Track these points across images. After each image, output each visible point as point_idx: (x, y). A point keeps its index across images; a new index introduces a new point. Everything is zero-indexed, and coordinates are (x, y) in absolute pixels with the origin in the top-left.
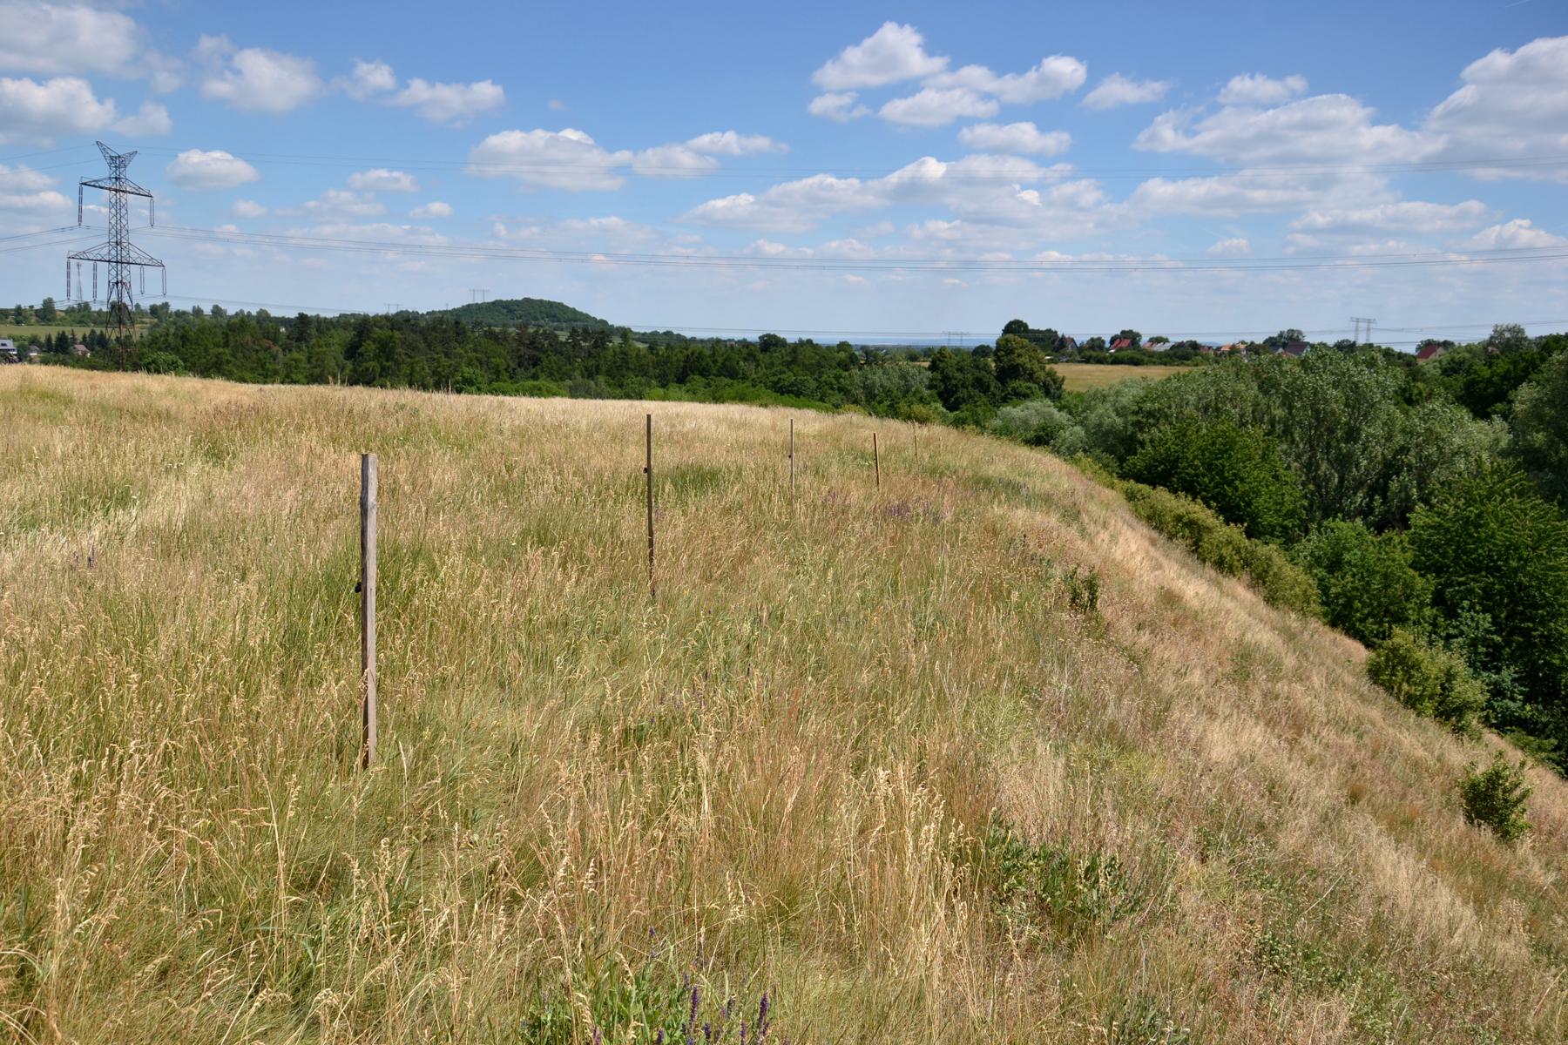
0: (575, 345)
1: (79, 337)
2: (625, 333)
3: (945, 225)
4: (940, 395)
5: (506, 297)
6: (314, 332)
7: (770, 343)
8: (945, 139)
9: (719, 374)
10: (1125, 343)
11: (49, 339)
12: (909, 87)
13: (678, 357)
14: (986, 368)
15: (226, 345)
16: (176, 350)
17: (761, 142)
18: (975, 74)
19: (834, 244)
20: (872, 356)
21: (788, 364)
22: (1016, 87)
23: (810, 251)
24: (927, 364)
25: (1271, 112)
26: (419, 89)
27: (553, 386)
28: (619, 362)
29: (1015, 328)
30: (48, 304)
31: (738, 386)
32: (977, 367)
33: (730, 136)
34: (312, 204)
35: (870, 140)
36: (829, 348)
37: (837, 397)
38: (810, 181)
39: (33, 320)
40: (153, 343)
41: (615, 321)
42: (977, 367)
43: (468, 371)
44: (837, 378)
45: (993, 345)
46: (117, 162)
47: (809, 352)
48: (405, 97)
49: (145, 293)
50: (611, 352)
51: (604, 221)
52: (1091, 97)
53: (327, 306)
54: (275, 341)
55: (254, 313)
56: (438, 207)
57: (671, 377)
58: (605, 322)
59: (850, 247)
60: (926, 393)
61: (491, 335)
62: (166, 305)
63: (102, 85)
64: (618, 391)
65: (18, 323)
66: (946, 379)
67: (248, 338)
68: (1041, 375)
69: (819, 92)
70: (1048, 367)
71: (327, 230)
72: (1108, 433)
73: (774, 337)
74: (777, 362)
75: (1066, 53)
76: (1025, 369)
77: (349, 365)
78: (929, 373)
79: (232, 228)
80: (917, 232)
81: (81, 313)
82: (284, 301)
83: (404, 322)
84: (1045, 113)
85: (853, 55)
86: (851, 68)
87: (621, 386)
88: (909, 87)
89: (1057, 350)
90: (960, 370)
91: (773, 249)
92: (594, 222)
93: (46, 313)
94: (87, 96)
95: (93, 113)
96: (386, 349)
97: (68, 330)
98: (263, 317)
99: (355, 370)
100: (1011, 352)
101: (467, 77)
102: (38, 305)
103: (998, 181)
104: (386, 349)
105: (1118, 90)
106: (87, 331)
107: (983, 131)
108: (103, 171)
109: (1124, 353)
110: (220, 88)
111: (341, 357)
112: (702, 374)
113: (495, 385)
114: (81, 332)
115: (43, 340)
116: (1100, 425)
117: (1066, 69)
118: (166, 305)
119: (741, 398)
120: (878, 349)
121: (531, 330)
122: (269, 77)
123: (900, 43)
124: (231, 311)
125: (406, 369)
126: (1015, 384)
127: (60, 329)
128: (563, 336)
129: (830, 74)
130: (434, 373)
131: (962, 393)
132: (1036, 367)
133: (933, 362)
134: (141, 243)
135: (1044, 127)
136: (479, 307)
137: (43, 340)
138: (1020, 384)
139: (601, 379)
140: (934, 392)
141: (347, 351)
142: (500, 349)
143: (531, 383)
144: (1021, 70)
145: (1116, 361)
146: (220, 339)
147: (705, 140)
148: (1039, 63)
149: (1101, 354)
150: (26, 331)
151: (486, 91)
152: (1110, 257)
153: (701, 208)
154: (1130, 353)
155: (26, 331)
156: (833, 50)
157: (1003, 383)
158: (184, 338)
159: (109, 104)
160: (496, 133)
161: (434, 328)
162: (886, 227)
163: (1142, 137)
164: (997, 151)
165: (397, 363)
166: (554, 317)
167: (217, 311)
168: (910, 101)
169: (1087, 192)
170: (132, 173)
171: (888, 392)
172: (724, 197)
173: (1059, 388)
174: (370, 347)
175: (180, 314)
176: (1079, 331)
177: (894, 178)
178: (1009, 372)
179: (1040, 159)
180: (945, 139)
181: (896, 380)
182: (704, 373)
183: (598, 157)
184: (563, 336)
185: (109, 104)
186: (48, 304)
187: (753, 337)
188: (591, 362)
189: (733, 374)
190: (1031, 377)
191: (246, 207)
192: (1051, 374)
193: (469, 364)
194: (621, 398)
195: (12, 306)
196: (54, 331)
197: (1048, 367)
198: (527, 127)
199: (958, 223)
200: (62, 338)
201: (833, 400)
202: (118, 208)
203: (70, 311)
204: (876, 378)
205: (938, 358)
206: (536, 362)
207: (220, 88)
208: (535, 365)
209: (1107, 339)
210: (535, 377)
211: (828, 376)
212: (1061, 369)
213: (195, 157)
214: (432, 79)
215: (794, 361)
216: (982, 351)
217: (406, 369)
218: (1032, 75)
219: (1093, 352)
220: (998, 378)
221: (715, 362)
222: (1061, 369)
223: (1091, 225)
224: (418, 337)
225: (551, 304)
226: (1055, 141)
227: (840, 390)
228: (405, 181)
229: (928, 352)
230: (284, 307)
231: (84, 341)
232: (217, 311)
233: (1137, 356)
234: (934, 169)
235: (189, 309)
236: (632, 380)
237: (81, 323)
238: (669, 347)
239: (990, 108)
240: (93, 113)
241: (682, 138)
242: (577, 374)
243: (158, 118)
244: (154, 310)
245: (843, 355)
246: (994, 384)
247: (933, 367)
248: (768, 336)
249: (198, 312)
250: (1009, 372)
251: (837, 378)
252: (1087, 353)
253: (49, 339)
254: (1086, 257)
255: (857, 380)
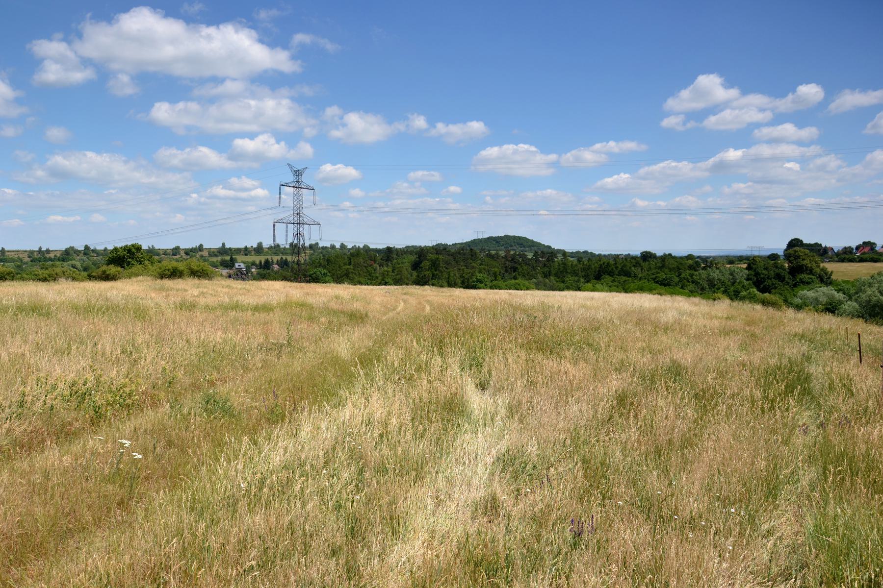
0: (537, 261)
1: (275, 261)
2: (564, 253)
3: (742, 185)
4: (754, 283)
5: (495, 234)
6: (395, 256)
7: (647, 256)
8: (743, 137)
9: (619, 275)
10: (866, 250)
11: (261, 263)
12: (716, 109)
13: (595, 266)
14: (782, 267)
15: (350, 264)
16: (324, 267)
17: (630, 145)
18: (757, 99)
19: (677, 199)
20: (708, 262)
21: (661, 268)
22: (785, 104)
23: (662, 203)
24: (745, 266)
25: (737, 111)
26: (441, 127)
27: (526, 283)
28: (562, 269)
29: (795, 243)
30: (260, 245)
31: (638, 283)
32: (777, 267)
33: (612, 144)
34: (388, 191)
35: (699, 140)
36: (681, 258)
37: (691, 287)
38: (662, 165)
39: (253, 253)
40: (312, 263)
41: (556, 246)
42: (777, 267)
43: (480, 276)
44: (691, 275)
45: (781, 253)
46: (298, 173)
47: (672, 261)
48: (433, 132)
49: (311, 237)
50: (557, 264)
51: (544, 192)
52: (833, 106)
53: (399, 243)
54: (375, 261)
55: (823, 246)
56: (452, 188)
57: (592, 277)
58: (549, 247)
59: (689, 200)
60: (746, 283)
61: (490, 256)
62: (317, 244)
63: (279, 136)
64: (562, 285)
65: (246, 255)
66: (757, 274)
67: (362, 260)
68: (818, 270)
69: (668, 114)
70: (822, 265)
71: (398, 202)
72: (874, 306)
73: (650, 252)
74: (652, 267)
75: (808, 82)
76: (807, 268)
77: (415, 273)
78: (746, 271)
79: (348, 204)
80: (727, 190)
81: (276, 249)
82: (378, 239)
83: (441, 249)
84: (801, 118)
85: (685, 94)
86: (684, 100)
87: (563, 282)
88: (716, 109)
89: (821, 255)
90: (766, 269)
91: (641, 203)
92: (539, 193)
93: (259, 250)
94: (273, 141)
95: (276, 149)
96: (435, 265)
97: (269, 258)
98: (366, 249)
99: (418, 276)
100: (799, 257)
101: (464, 120)
102: (255, 246)
103: (774, 159)
104: (435, 265)
105: (852, 100)
106: (279, 258)
107: (766, 131)
108: (290, 178)
109: (867, 256)
110: (336, 134)
111: (410, 269)
112: (609, 274)
113: (495, 283)
114: (276, 258)
115: (258, 263)
116: (870, 301)
117: (811, 91)
118: (317, 244)
119: (641, 289)
120: (715, 258)
121: (512, 252)
122: (363, 127)
123: (710, 84)
124: (349, 247)
125: (445, 275)
126: (802, 276)
127: (266, 257)
128: (530, 255)
129: (671, 103)
130: (461, 277)
131: (768, 282)
132: (814, 265)
133: (749, 265)
134: (309, 213)
135: (800, 125)
136: (480, 241)
137: (258, 263)
138: (805, 276)
139: (552, 278)
140: (751, 282)
141: (413, 266)
142: (495, 263)
143: (513, 281)
144: (783, 95)
145: (862, 260)
146: (346, 261)
147: (598, 146)
148: (794, 91)
149: (852, 257)
150: (250, 259)
151: (476, 126)
152: (848, 200)
153: (599, 183)
154: (871, 255)
155: (250, 259)
156: (673, 91)
157: (794, 276)
158: (328, 261)
159: (283, 143)
160: (484, 149)
161: (459, 253)
162: (708, 188)
163: (869, 125)
164: (774, 141)
165: (441, 272)
166: (521, 245)
167: (343, 246)
168: (717, 116)
169: (832, 162)
170: (305, 179)
171: (723, 283)
172: (611, 176)
173: (829, 278)
174: (426, 264)
175: (324, 248)
176: (836, 243)
177: (711, 161)
178: (796, 270)
179: (800, 143)
180: (743, 137)
181: (727, 276)
182: (611, 274)
183: (540, 158)
184: (530, 255)
185: (283, 143)
186: (260, 245)
187: (638, 253)
188: (546, 269)
189: (628, 274)
190: (811, 272)
191: (357, 192)
192: (824, 270)
193: (480, 272)
194: (563, 290)
195: (243, 247)
196: (262, 258)
197: (822, 265)
198: (500, 144)
199: (750, 184)
200: (267, 262)
201: (689, 288)
202: (298, 198)
203: (270, 248)
204: (715, 275)
205: (751, 262)
206: (515, 269)
207: (336, 134)
208: (514, 271)
209: (854, 247)
210: (515, 278)
211: (686, 274)
212: (830, 266)
213: (328, 168)
214: (447, 122)
215: (663, 266)
216: (774, 257)
217: (445, 275)
218: (790, 96)
219: (846, 255)
220: (789, 273)
221: (617, 268)
222: (830, 266)
223: (834, 181)
224: (451, 258)
225: (520, 238)
226: (809, 132)
227: (693, 282)
228: (436, 176)
229: (747, 258)
230: (378, 243)
231: (277, 263)
232: (343, 246)
233: (876, 256)
234: (733, 154)
235: (329, 246)
236: (570, 279)
237: (276, 254)
238: (589, 260)
239: (768, 116)
240: (276, 149)
241: (589, 144)
242: (539, 276)
243: (307, 149)
244: (311, 246)
245: (690, 262)
246: (788, 278)
247: (749, 268)
248: (646, 252)
249: (333, 247)
250: (796, 270)
251: (691, 275)
252: (843, 256)
253: (261, 263)
254: (833, 200)
255: (704, 276)
